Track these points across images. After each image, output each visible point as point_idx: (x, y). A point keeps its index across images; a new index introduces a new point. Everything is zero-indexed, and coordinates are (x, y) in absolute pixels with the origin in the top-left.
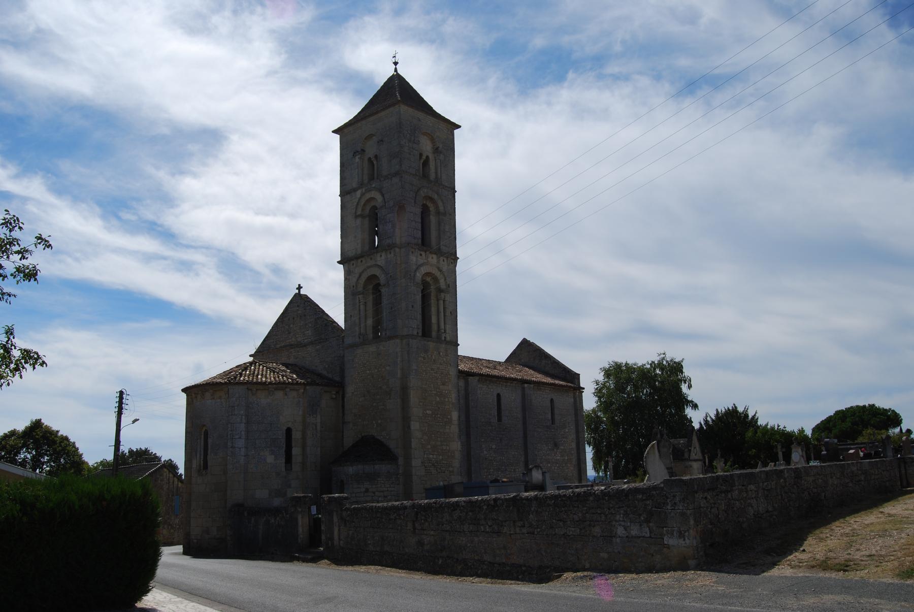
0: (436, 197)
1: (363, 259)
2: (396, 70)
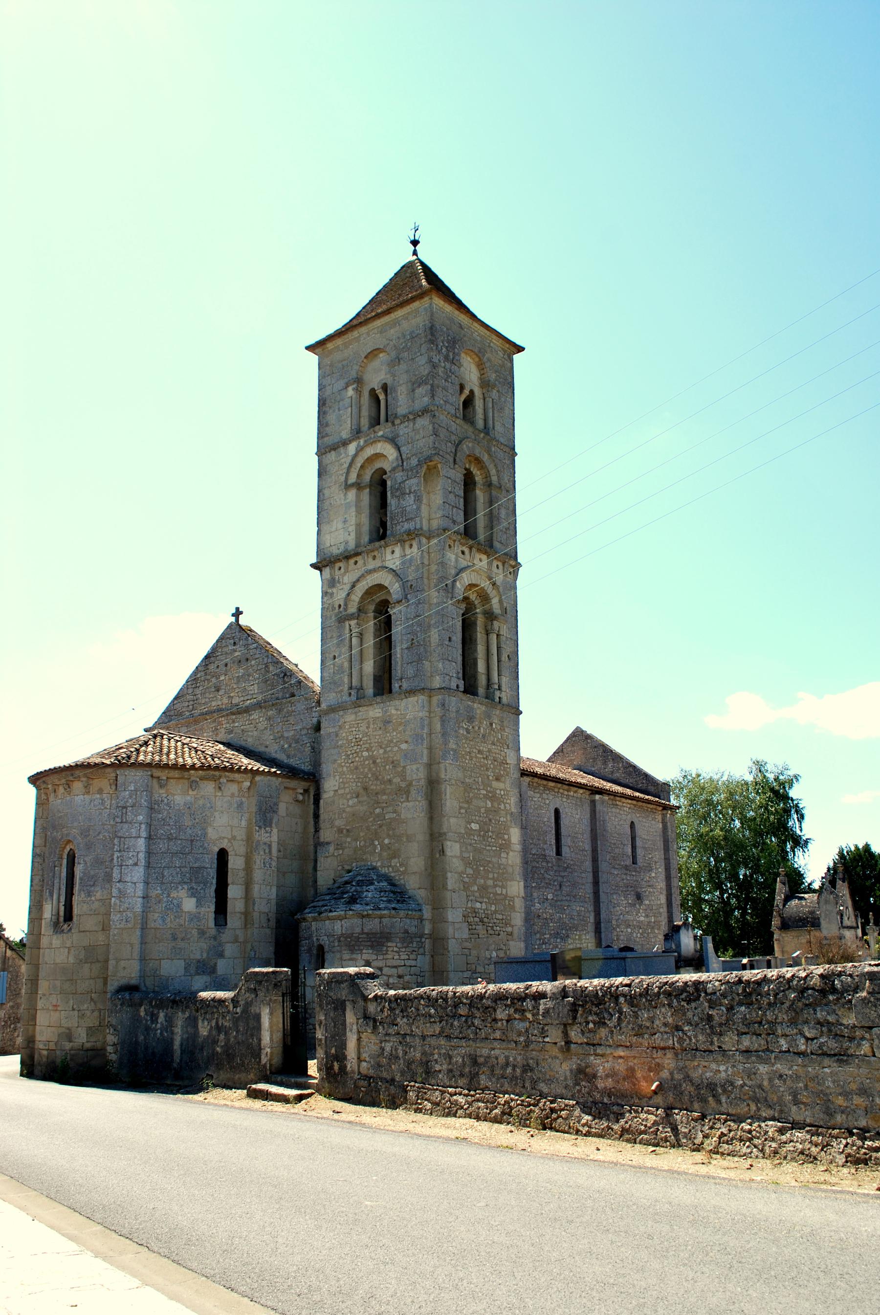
0: (485, 458)
1: (359, 559)
2: (415, 253)
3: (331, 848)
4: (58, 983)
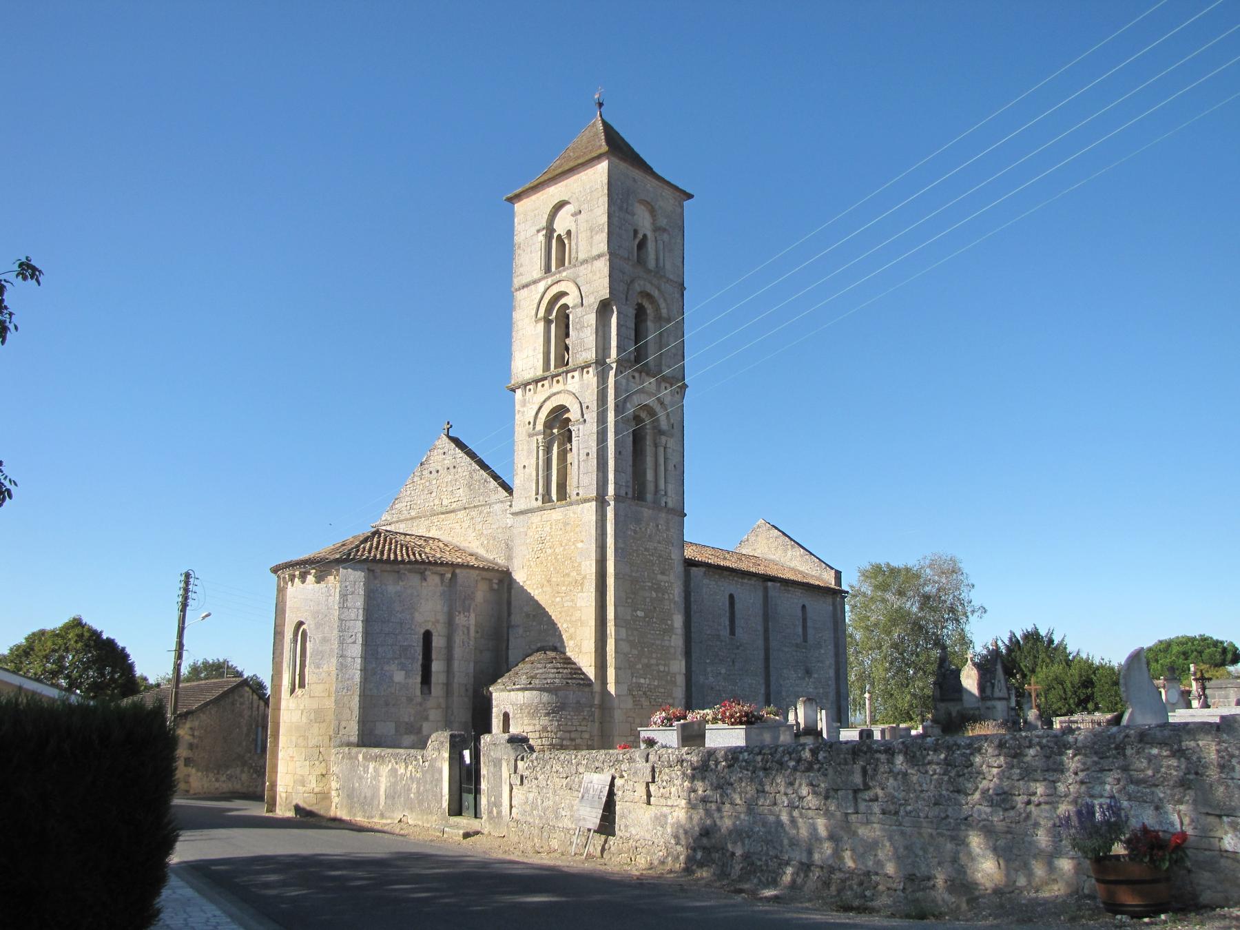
0: (656, 294)
3: (521, 631)
4: (294, 739)
